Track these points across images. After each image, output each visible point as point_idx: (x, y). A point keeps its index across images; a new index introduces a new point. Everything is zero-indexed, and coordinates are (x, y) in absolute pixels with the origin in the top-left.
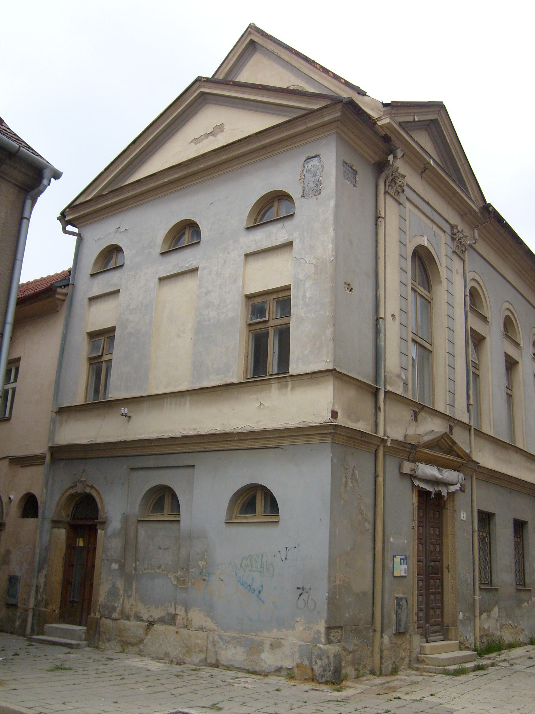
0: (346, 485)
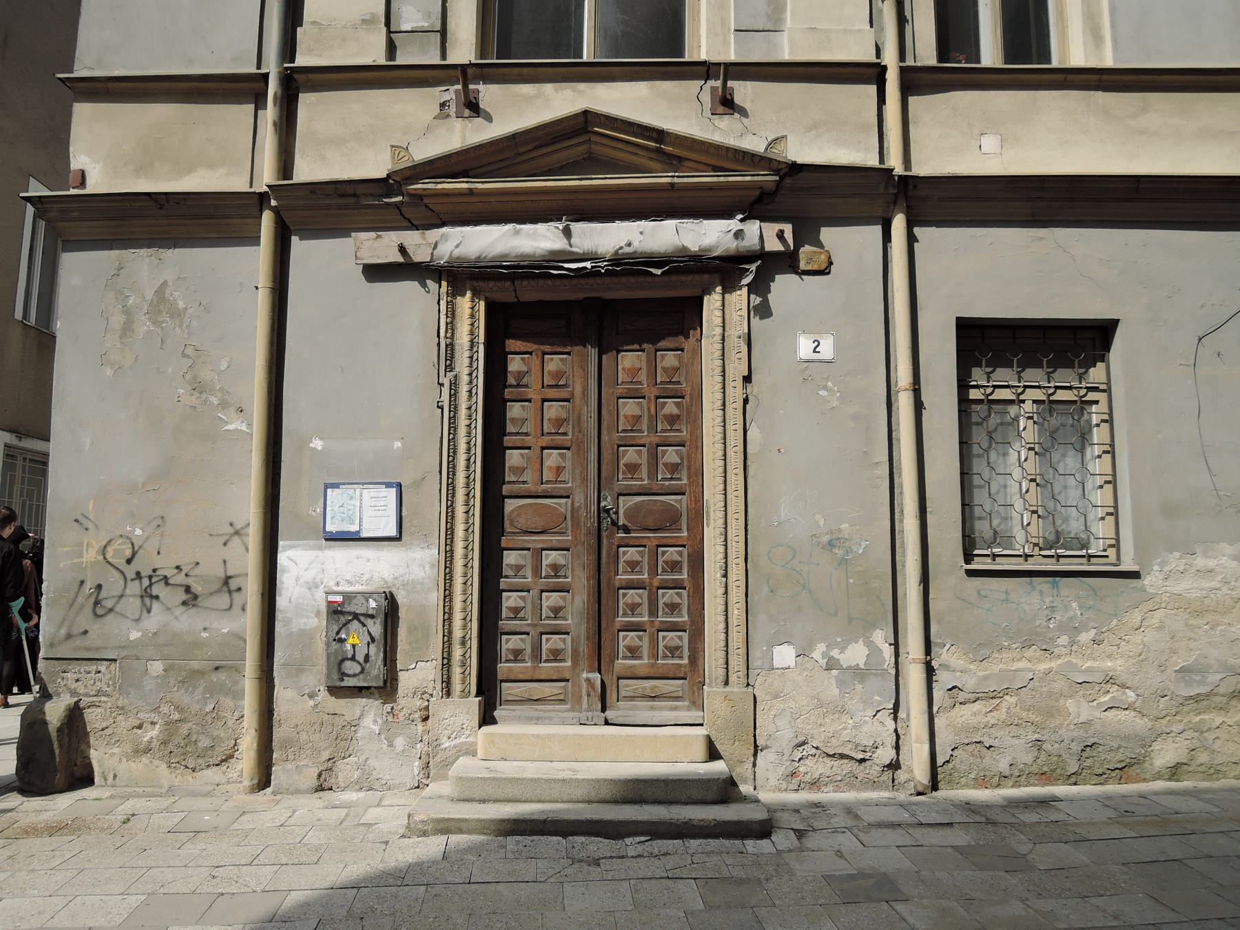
0: (127, 328)
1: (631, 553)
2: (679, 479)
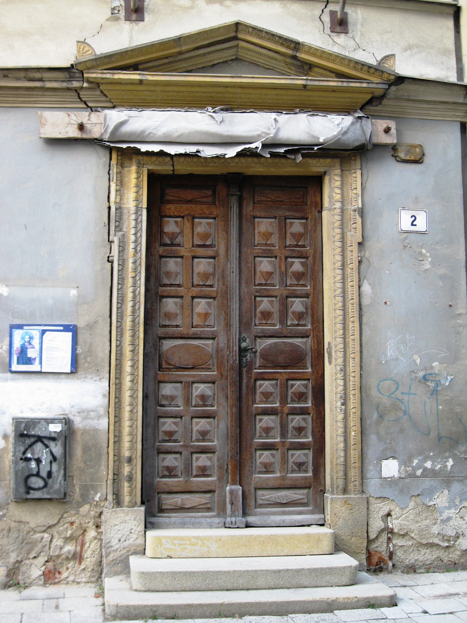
1: (265, 386)
2: (304, 325)
